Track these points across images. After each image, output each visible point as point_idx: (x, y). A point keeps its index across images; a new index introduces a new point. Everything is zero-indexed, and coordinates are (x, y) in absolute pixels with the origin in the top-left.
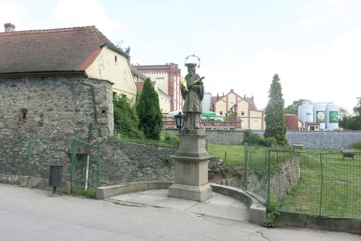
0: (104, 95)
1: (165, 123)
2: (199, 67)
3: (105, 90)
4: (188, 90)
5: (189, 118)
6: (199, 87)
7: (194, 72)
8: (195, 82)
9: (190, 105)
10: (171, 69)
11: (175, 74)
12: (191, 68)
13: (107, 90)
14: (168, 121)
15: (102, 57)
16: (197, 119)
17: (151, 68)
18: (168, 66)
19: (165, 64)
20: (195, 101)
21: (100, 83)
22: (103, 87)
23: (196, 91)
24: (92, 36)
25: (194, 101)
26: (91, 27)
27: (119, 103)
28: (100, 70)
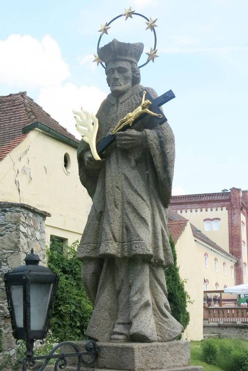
0: (13, 242)
1: (221, 312)
2: (152, 57)
3: (18, 230)
4: (97, 157)
5: (103, 287)
6: (145, 138)
7: (136, 80)
8: (132, 115)
9: (107, 228)
10: (232, 201)
11: (241, 209)
12: (115, 60)
13: (22, 228)
14: (227, 309)
15: (26, 152)
16: (141, 291)
17: (194, 200)
18: (228, 194)
19: (220, 191)
20: (129, 203)
21: (6, 211)
22: (13, 220)
23: (137, 162)
24: (14, 112)
25: (126, 206)
26: (18, 94)
27: (70, 264)
28: (17, 183)
